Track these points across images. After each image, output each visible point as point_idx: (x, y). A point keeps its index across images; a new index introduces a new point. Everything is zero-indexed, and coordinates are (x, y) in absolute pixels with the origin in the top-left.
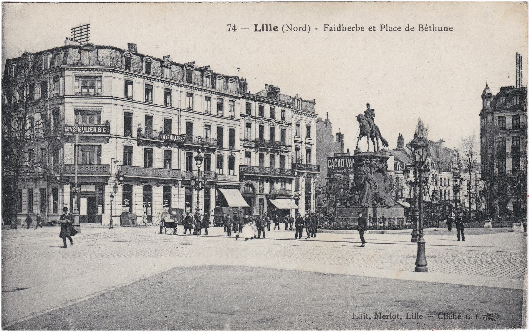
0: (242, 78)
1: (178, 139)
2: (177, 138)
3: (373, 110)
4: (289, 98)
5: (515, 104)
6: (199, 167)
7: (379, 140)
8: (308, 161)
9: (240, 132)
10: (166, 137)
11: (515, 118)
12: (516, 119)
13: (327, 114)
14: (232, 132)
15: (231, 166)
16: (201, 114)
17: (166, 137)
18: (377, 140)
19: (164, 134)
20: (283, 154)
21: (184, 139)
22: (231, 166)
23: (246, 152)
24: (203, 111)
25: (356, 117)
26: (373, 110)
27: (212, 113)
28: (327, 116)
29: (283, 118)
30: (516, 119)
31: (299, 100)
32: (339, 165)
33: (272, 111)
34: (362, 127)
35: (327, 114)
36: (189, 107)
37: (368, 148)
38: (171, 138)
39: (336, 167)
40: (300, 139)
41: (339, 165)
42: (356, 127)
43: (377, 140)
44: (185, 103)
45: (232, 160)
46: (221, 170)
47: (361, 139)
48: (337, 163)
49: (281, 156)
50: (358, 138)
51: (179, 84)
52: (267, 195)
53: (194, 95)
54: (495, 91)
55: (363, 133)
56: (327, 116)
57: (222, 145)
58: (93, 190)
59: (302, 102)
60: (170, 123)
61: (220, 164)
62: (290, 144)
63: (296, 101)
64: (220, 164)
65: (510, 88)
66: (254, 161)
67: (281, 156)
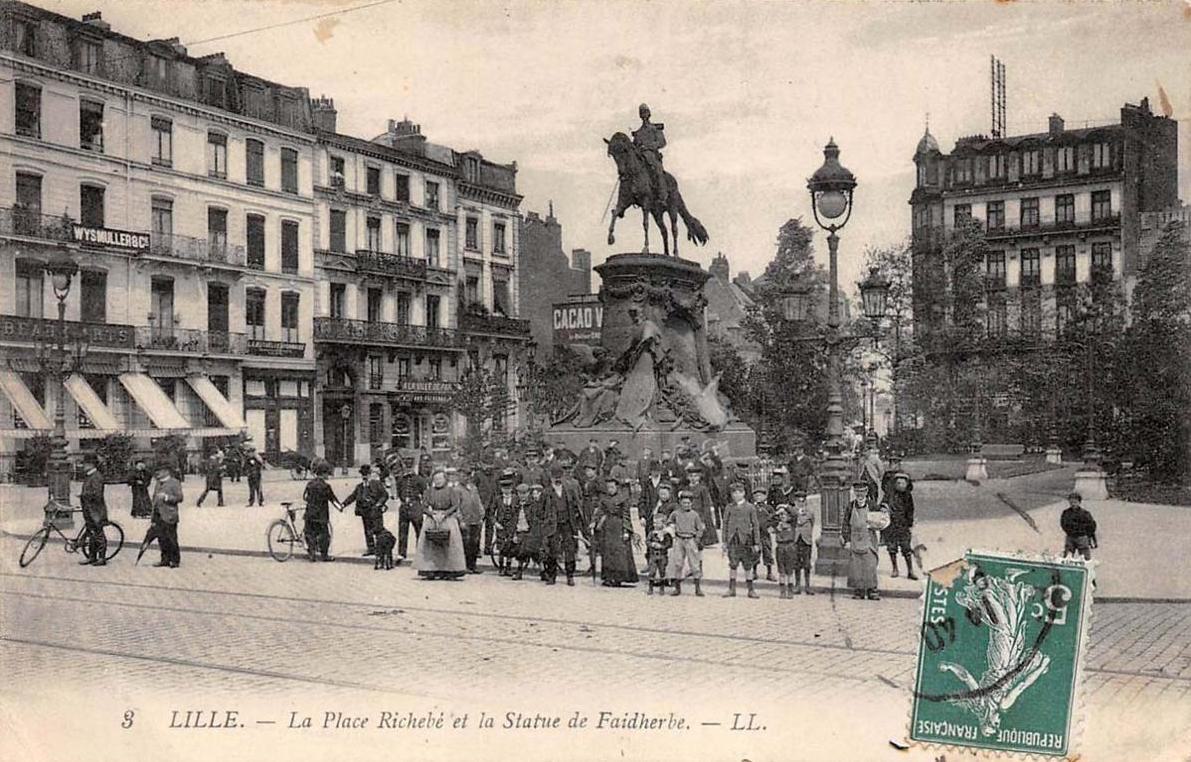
0: (323, 97)
1: (124, 242)
2: (122, 239)
3: (661, 127)
4: (450, 154)
5: (992, 175)
6: (62, 298)
7: (680, 223)
8: (374, 243)
9: (313, 235)
10: (84, 234)
11: (993, 208)
12: (997, 212)
13: (551, 206)
14: (290, 230)
15: (290, 317)
16: (195, 179)
17: (84, 234)
18: (674, 221)
19: (81, 226)
20: (434, 292)
21: (143, 242)
22: (290, 317)
23: (333, 285)
24: (203, 172)
25: (606, 141)
26: (661, 127)
27: (231, 177)
28: (551, 210)
29: (433, 203)
30: (997, 212)
31: (476, 161)
32: (580, 322)
33: (402, 183)
34: (626, 176)
35: (551, 206)
36: (160, 158)
37: (647, 244)
38: (102, 237)
39: (572, 326)
40: (478, 257)
41: (580, 322)
42: (608, 174)
43: (674, 221)
44: (144, 147)
45: (290, 301)
46: (259, 329)
47: (621, 215)
48: (574, 318)
49: (429, 297)
50: (613, 211)
51: (126, 92)
52: (390, 394)
53: (174, 126)
54: (946, 147)
55: (629, 197)
56: (551, 210)
57: (262, 262)
58: (291, 394)
59: (484, 167)
60: (100, 200)
61: (255, 315)
62: (452, 268)
63: (467, 162)
64: (255, 315)
65: (980, 139)
66: (354, 305)
67: (429, 297)
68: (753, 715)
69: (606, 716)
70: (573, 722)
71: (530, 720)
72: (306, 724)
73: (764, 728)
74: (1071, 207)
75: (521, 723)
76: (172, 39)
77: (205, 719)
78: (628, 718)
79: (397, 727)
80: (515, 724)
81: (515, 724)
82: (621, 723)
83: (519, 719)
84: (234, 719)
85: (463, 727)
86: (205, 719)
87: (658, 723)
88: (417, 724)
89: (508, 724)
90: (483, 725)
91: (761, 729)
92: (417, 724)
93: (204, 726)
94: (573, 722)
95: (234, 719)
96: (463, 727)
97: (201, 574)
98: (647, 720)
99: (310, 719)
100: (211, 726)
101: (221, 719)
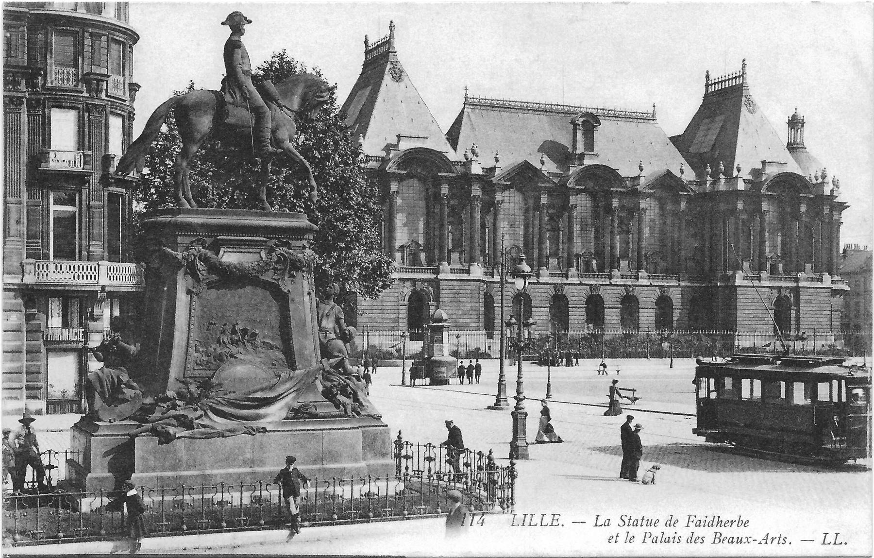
68: (543, 515)
69: (556, 517)
70: (669, 522)
71: (637, 520)
72: (606, 524)
73: (846, 544)
74: (604, 132)
75: (663, 540)
76: (543, 3)
77: (537, 520)
78: (708, 520)
79: (672, 526)
80: (627, 524)
81: (627, 524)
82: (735, 540)
83: (630, 520)
84: (557, 520)
85: (616, 542)
86: (537, 520)
87: (730, 523)
88: (723, 524)
89: (622, 523)
90: (663, 540)
91: (843, 544)
92: (723, 524)
93: (841, 544)
94: (669, 522)
95: (557, 520)
96: (616, 542)
97: (628, 159)
98: (722, 521)
99: (609, 520)
100: (835, 544)
101: (548, 519)
